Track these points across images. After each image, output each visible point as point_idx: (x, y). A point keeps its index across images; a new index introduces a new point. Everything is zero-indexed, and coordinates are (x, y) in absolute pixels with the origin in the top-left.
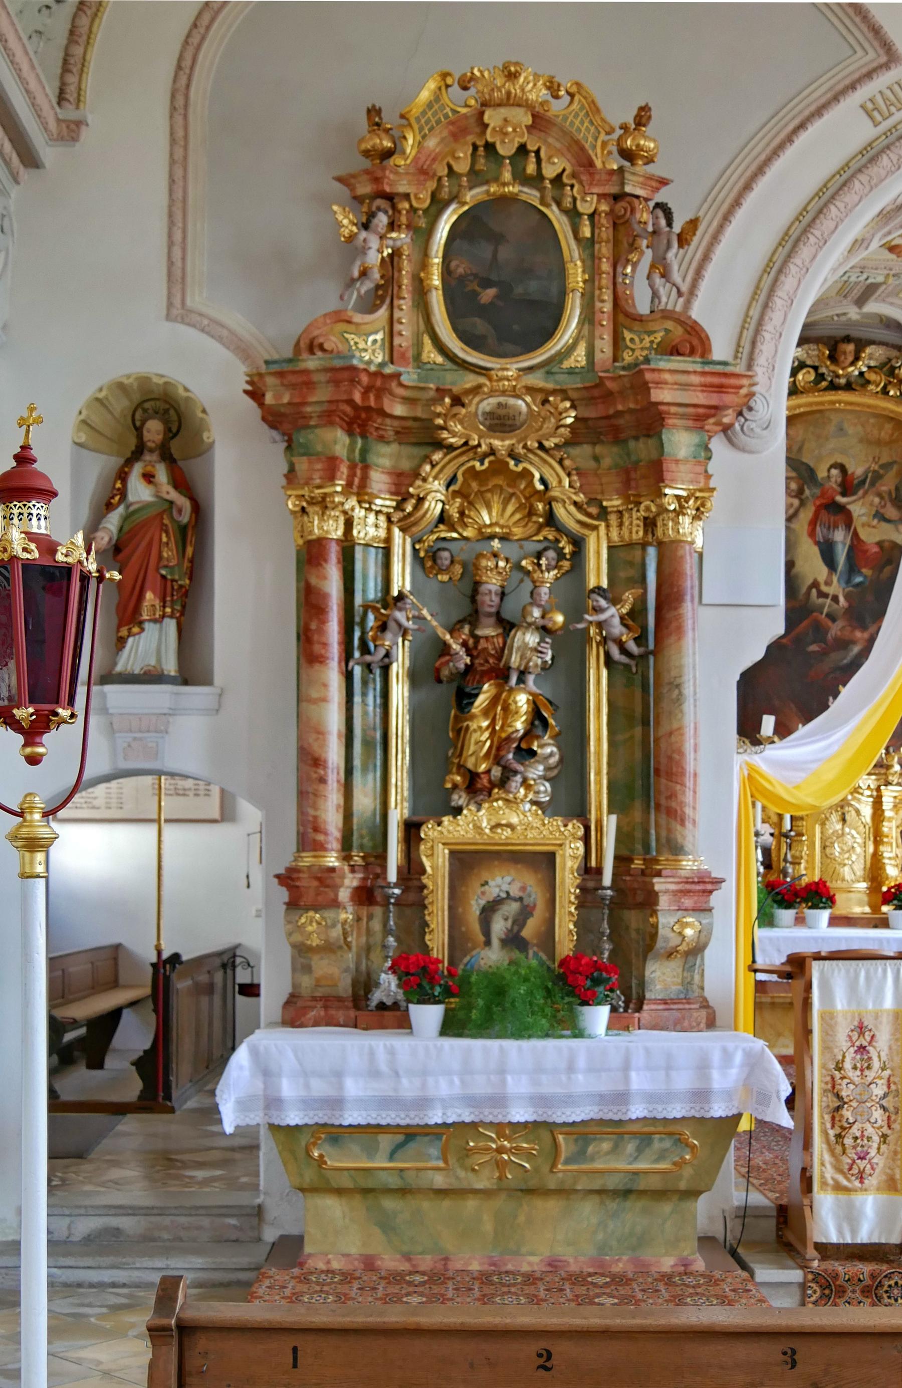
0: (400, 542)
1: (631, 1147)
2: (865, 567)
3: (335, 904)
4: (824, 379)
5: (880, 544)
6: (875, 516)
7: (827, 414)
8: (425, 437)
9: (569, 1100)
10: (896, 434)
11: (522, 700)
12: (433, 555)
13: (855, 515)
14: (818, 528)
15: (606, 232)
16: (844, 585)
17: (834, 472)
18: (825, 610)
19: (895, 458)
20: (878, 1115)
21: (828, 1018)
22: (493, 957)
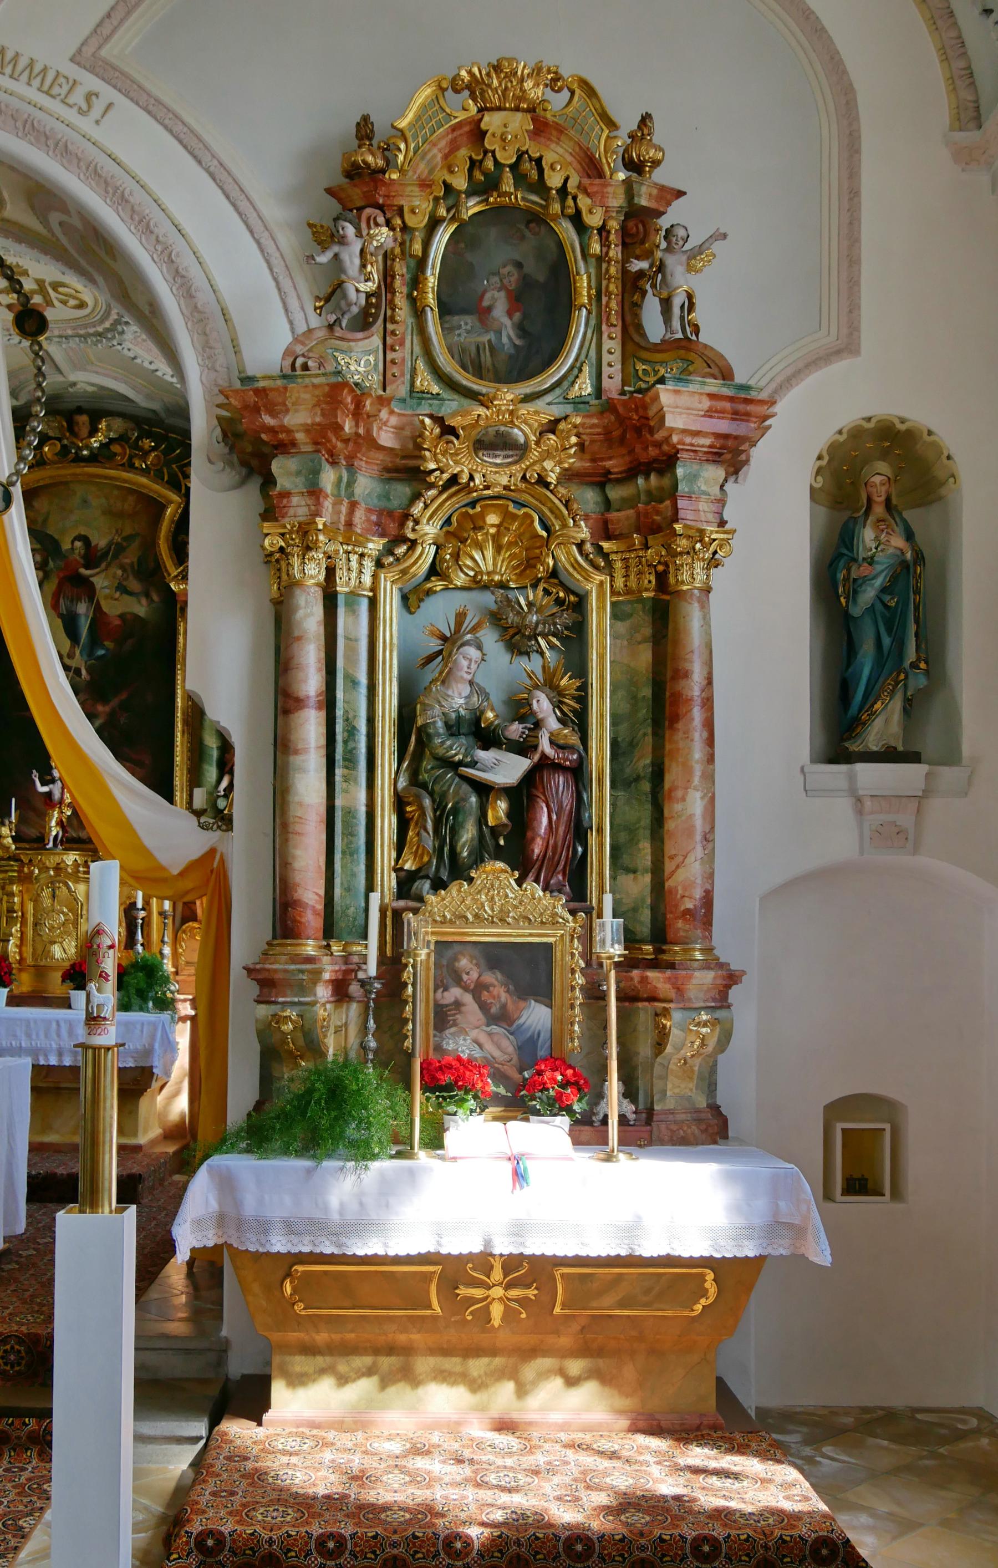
5: (122, 616)
6: (117, 589)
13: (98, 587)
14: (61, 601)
16: (85, 657)
17: (78, 544)
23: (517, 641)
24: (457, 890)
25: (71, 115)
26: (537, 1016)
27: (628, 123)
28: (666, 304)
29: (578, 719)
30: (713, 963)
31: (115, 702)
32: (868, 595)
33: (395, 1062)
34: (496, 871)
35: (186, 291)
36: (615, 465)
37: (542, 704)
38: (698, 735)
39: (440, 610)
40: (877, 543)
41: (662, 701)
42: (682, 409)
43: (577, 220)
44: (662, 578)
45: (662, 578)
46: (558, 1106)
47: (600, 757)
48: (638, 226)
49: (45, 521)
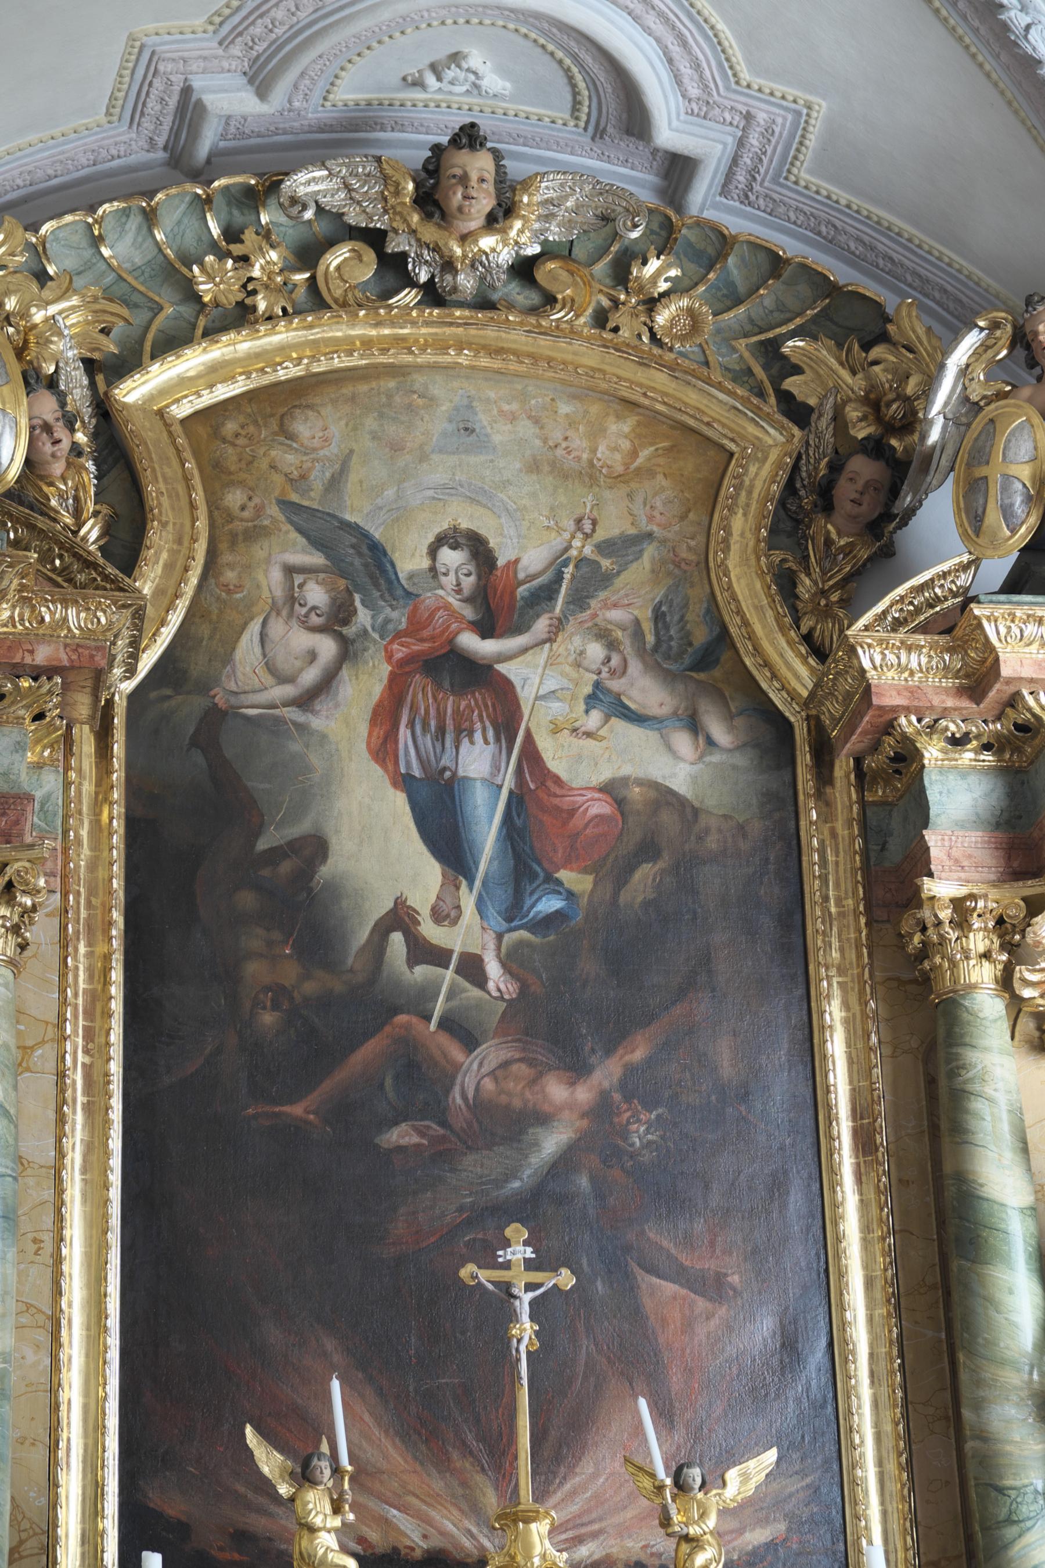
2: (566, 864)
4: (410, 282)
5: (610, 789)
6: (592, 700)
7: (419, 380)
10: (645, 453)
13: (526, 695)
14: (404, 733)
16: (497, 922)
17: (451, 558)
18: (439, 1008)
19: (645, 526)
31: (607, 1073)
49: (335, 484)
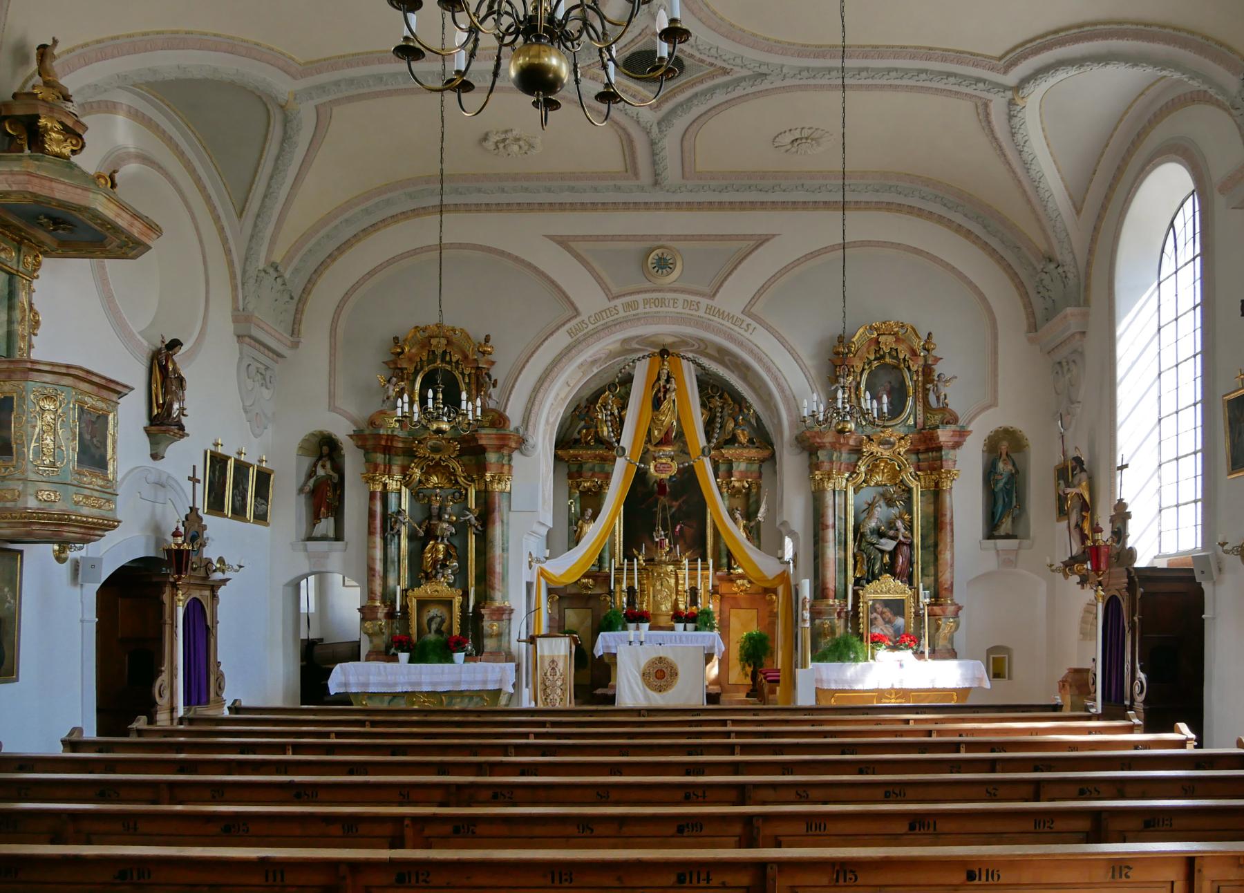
0: (405, 492)
1: (467, 700)
3: (376, 619)
8: (410, 453)
9: (441, 683)
11: (441, 547)
12: (417, 494)
15: (473, 380)
20: (559, 691)
21: (542, 657)
22: (432, 637)
23: (890, 503)
24: (875, 584)
25: (742, 332)
26: (900, 621)
27: (924, 337)
28: (938, 398)
29: (910, 528)
30: (953, 604)
32: (1001, 484)
33: (861, 637)
34: (887, 577)
35: (782, 390)
36: (922, 448)
37: (899, 524)
38: (949, 534)
39: (868, 494)
40: (1003, 467)
41: (937, 523)
42: (944, 435)
43: (909, 368)
44: (937, 484)
45: (937, 484)
46: (909, 647)
47: (917, 540)
48: (927, 371)
